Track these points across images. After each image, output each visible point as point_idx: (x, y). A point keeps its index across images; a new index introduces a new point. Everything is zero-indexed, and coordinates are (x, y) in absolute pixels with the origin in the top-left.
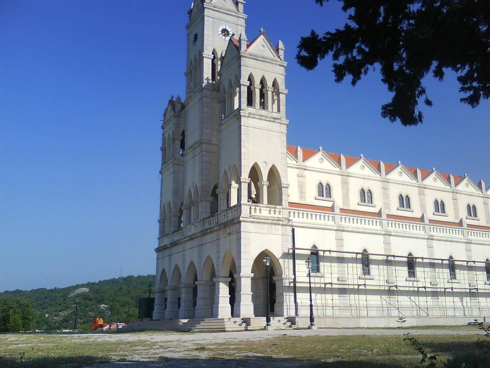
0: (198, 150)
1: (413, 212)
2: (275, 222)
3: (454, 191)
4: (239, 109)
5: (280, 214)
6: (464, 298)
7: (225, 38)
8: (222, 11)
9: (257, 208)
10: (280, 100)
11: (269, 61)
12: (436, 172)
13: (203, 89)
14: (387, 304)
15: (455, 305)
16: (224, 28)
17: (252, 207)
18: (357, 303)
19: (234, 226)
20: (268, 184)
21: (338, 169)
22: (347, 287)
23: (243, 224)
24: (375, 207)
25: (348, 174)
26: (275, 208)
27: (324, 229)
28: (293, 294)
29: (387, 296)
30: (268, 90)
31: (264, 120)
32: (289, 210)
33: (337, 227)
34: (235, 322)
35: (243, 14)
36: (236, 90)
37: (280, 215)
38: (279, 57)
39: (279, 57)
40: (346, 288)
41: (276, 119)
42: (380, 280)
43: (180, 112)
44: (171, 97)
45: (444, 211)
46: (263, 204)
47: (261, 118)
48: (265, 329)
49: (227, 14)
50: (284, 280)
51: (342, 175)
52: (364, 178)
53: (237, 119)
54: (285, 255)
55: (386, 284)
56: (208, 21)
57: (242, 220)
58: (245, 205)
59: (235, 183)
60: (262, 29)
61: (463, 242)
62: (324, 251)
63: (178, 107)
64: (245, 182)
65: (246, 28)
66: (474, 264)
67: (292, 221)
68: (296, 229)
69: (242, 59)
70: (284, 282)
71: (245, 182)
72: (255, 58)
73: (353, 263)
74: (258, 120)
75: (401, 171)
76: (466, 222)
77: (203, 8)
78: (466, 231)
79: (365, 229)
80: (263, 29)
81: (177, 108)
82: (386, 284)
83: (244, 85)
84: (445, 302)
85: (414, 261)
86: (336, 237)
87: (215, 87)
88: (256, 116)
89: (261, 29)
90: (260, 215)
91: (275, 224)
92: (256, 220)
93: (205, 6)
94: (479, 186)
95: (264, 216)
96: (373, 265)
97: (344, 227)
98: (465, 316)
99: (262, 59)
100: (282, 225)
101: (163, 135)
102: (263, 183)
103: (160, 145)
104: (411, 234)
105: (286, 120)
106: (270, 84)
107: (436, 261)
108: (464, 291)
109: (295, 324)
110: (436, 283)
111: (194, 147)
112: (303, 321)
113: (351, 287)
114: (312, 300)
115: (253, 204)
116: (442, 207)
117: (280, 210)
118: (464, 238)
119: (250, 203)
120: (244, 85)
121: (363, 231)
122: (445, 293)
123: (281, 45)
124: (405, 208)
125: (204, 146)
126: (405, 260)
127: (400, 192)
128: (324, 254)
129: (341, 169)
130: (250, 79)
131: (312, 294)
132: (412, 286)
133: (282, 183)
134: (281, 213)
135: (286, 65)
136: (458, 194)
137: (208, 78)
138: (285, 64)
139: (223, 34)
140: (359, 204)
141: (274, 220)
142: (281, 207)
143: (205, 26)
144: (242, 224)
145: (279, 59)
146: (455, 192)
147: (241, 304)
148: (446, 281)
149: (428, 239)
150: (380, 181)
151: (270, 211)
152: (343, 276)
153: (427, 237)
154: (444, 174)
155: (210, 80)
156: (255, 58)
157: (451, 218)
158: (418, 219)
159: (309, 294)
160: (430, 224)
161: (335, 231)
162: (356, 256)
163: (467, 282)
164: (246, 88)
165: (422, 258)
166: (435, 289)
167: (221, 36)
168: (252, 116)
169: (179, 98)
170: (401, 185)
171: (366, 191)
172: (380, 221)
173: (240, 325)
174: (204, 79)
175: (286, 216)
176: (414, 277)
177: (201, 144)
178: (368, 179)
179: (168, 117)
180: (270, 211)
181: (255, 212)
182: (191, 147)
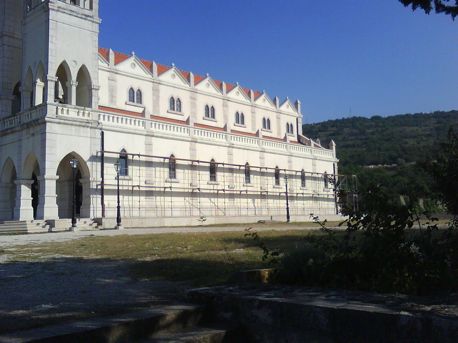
2: (84, 124)
9: (64, 108)
14: (190, 205)
19: (38, 126)
20: (77, 84)
21: (150, 76)
22: (154, 189)
27: (134, 134)
33: (147, 132)
34: (38, 224)
40: (153, 191)
42: (184, 183)
45: (243, 123)
50: (91, 183)
51: (153, 82)
52: (174, 87)
53: (45, 11)
54: (93, 158)
55: (190, 187)
57: (48, 120)
58: (51, 104)
61: (258, 151)
62: (133, 155)
67: (101, 124)
74: (68, 16)
76: (263, 133)
78: (313, 150)
79: (135, 130)
82: (190, 187)
88: (66, 11)
91: (84, 126)
92: (63, 121)
100: (91, 128)
102: (72, 83)
105: (99, 19)
107: (234, 167)
110: (233, 186)
112: (109, 222)
113: (158, 189)
115: (61, 104)
116: (213, 112)
121: (172, 137)
122: (240, 196)
127: (264, 116)
129: (152, 76)
134: (91, 115)
142: (90, 109)
144: (48, 124)
146: (279, 113)
151: (78, 112)
153: (228, 145)
158: (139, 113)
159: (117, 196)
160: (314, 148)
163: (259, 186)
168: (62, 10)
170: (172, 88)
175: (96, 119)
180: (78, 112)
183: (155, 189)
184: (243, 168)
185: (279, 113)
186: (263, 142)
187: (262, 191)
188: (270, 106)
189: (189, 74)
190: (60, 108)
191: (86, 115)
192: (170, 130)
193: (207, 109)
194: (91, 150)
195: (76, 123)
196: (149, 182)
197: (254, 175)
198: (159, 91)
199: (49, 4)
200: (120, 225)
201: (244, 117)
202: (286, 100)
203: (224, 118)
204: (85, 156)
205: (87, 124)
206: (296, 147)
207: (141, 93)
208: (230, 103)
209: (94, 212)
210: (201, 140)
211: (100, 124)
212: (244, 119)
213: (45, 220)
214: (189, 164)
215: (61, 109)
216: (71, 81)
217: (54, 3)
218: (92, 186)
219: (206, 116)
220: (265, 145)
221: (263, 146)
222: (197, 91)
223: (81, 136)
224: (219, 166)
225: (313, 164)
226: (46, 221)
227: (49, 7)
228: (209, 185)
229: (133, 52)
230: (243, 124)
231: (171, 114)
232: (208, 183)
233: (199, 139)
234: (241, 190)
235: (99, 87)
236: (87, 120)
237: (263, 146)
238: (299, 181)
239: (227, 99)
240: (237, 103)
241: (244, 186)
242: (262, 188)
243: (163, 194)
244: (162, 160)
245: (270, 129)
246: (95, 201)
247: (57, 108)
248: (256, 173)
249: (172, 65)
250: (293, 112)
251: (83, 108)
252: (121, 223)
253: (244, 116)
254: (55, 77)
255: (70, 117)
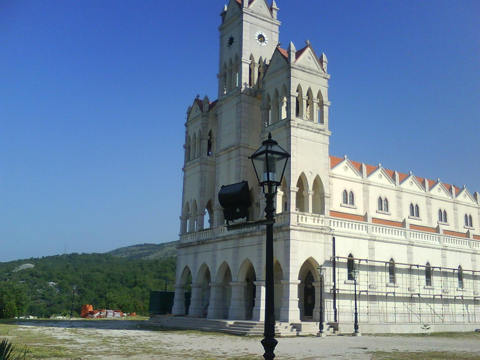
0: (234, 153)
1: (390, 215)
2: (319, 231)
3: (456, 202)
4: (289, 119)
5: (322, 223)
6: (469, 305)
7: (261, 44)
8: (259, 16)
9: (303, 216)
10: (324, 112)
11: (315, 73)
12: (347, 160)
13: (241, 93)
14: (409, 310)
15: (396, 310)
16: (261, 34)
17: (299, 215)
18: (385, 309)
19: (281, 233)
20: (313, 194)
21: (360, 178)
22: (376, 294)
23: (292, 232)
24: (421, 220)
25: (368, 183)
26: (319, 217)
27: (359, 238)
28: (333, 301)
29: (408, 303)
30: (314, 102)
31: (310, 131)
32: (330, 219)
33: (370, 236)
34: (286, 327)
35: (276, 21)
36: (283, 100)
37: (323, 224)
38: (323, 69)
39: (323, 69)
40: (375, 295)
41: (321, 130)
42: (403, 288)
43: (208, 112)
44: (197, 96)
45: (352, 203)
46: (308, 212)
47: (308, 128)
48: (318, 335)
49: (263, 20)
50: (325, 287)
51: (363, 183)
52: (382, 187)
53: (286, 128)
54: (327, 263)
55: (408, 292)
56: (246, 26)
57: (292, 228)
58: (294, 213)
59: (281, 191)
60: (308, 41)
61: (470, 253)
62: (360, 260)
63: (206, 107)
64: (294, 191)
65: (279, 34)
66: (417, 268)
67: (333, 230)
68: (336, 238)
69: (292, 70)
70: (325, 289)
71: (294, 191)
72: (304, 70)
73: (382, 271)
74: (305, 131)
75: (347, 165)
76: (409, 221)
77: (242, 13)
78: (442, 238)
79: (361, 235)
80: (309, 42)
81: (205, 109)
82: (408, 292)
83: (294, 96)
84: (386, 307)
85: (431, 270)
86: (368, 246)
87: (256, 92)
88: (303, 127)
89: (307, 41)
90: (306, 223)
91: (319, 233)
92: (303, 228)
93: (243, 11)
94: (393, 177)
95: (310, 225)
96: (415, 275)
97: (477, 251)
98: (470, 322)
99: (309, 71)
100: (325, 234)
101: (187, 133)
102: (309, 193)
103: (183, 142)
104: (429, 244)
105: (329, 132)
106: (315, 95)
107: (448, 271)
108: (469, 299)
109: (338, 330)
110: (448, 291)
111: (230, 150)
112: (346, 327)
113: (380, 294)
114: (357, 309)
115: (301, 213)
116: (412, 210)
117: (323, 219)
118: (470, 249)
119: (298, 212)
120: (294, 96)
121: (391, 240)
122: (455, 301)
123: (325, 58)
124: (348, 205)
125: (242, 150)
126: (424, 269)
127: (411, 201)
128: (359, 262)
129: (363, 178)
130: (299, 90)
131: (357, 301)
132: (428, 294)
133: (325, 193)
134: (324, 221)
135: (329, 78)
136: (457, 204)
137: (246, 83)
138: (329, 77)
139: (260, 40)
140: (378, 212)
141: (318, 229)
142: (323, 216)
143: (243, 31)
144: (292, 232)
145: (323, 72)
146: (366, 184)
147: (261, 309)
148: (422, 287)
149: (442, 249)
150: (395, 190)
151: (314, 219)
152: (374, 284)
153: (442, 247)
154: (419, 178)
155: (247, 85)
156: (303, 69)
157: (393, 217)
158: (464, 233)
159: (354, 301)
160: (474, 240)
161: (368, 241)
162: (386, 265)
163: (472, 290)
164: (295, 99)
165: (418, 266)
166: (425, 296)
167: (258, 42)
168: (300, 127)
169: (206, 98)
170: (380, 188)
171: (383, 199)
172: (356, 224)
173: (292, 331)
174: (242, 83)
175: (328, 225)
176: (431, 285)
177: (239, 147)
178: (385, 188)
179: (193, 114)
180: (314, 219)
181: (302, 220)
182: (226, 149)
183: (378, 294)
184: (456, 271)
185: (366, 184)
186: (444, 238)
187: (475, 296)
188: (472, 202)
189: (362, 166)
190: (300, 216)
191: (320, 222)
192: (348, 228)
193: (346, 194)
194: (324, 256)
195: (313, 229)
196: (372, 286)
197: (467, 279)
198: (369, 192)
199: (291, 122)
200: (322, 332)
201: (447, 214)
202: (437, 182)
203: (428, 216)
204: (321, 262)
205: (322, 230)
206: (446, 239)
207: (353, 195)
208: (432, 200)
209: (328, 316)
210: (418, 243)
211: (332, 230)
212: (472, 221)
213: (290, 322)
214: (407, 267)
215: (301, 217)
216: (309, 191)
217: (294, 121)
218: (403, 294)
219: (379, 209)
220: (376, 232)
221: (373, 233)
222: (402, 190)
223: (317, 242)
224: (435, 269)
225: (370, 247)
226: (291, 324)
227: (291, 124)
228: (425, 290)
229: (346, 155)
230: (446, 222)
231: (379, 214)
232: (424, 287)
233: (415, 242)
234: (387, 291)
235: (330, 195)
236: (322, 226)
237: (373, 233)
238: (423, 277)
239: (430, 196)
240: (440, 200)
241: (458, 291)
242: (476, 293)
243: (386, 298)
244: (384, 264)
245: (472, 226)
246: (328, 304)
247: (298, 216)
248: (468, 277)
249: (345, 157)
250: (471, 202)
251: (318, 215)
252: (358, 330)
253: (447, 213)
254: (297, 188)
255: (308, 225)
